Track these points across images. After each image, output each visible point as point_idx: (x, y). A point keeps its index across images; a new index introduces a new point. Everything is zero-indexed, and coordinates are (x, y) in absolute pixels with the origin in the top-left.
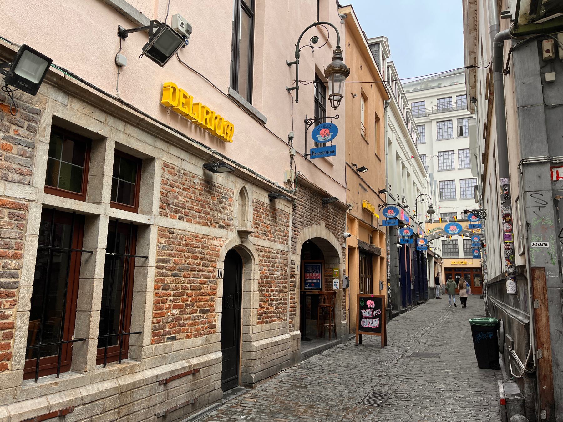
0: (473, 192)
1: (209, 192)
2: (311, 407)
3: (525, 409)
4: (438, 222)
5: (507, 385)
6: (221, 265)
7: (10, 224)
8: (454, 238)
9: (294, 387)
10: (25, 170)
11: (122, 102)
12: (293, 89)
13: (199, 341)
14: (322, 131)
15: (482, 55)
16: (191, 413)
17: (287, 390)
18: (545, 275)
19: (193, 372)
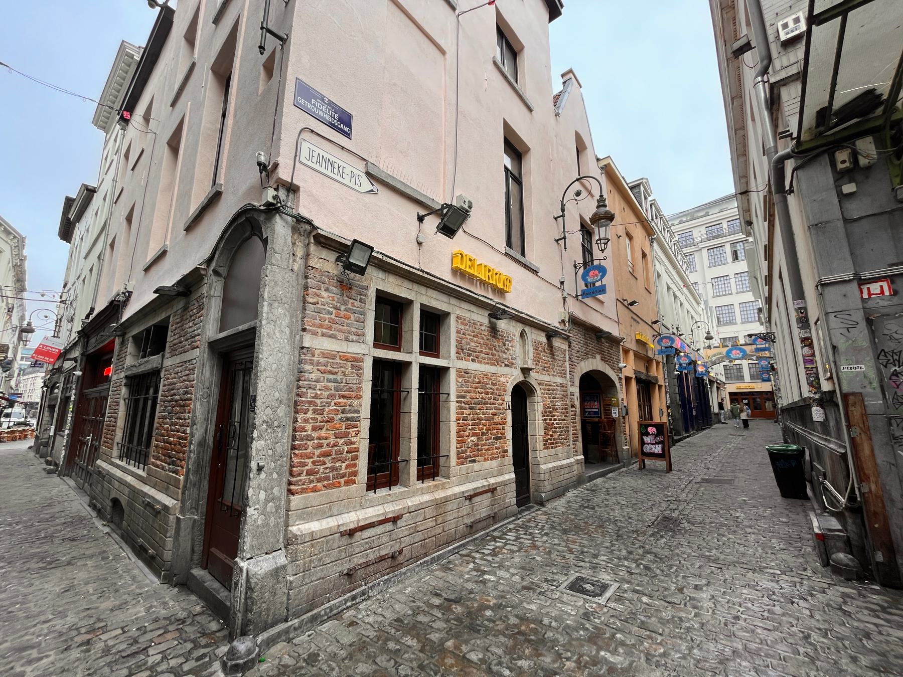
0: (756, 315)
1: (494, 337)
2: (600, 526)
3: (851, 548)
4: (718, 347)
5: (822, 519)
6: (508, 399)
7: (352, 373)
8: (737, 362)
9: (582, 507)
10: (360, 332)
11: (423, 271)
12: (562, 239)
13: (494, 464)
14: (591, 273)
15: (755, 178)
16: (493, 525)
17: (576, 510)
18: (863, 401)
19: (492, 490)
